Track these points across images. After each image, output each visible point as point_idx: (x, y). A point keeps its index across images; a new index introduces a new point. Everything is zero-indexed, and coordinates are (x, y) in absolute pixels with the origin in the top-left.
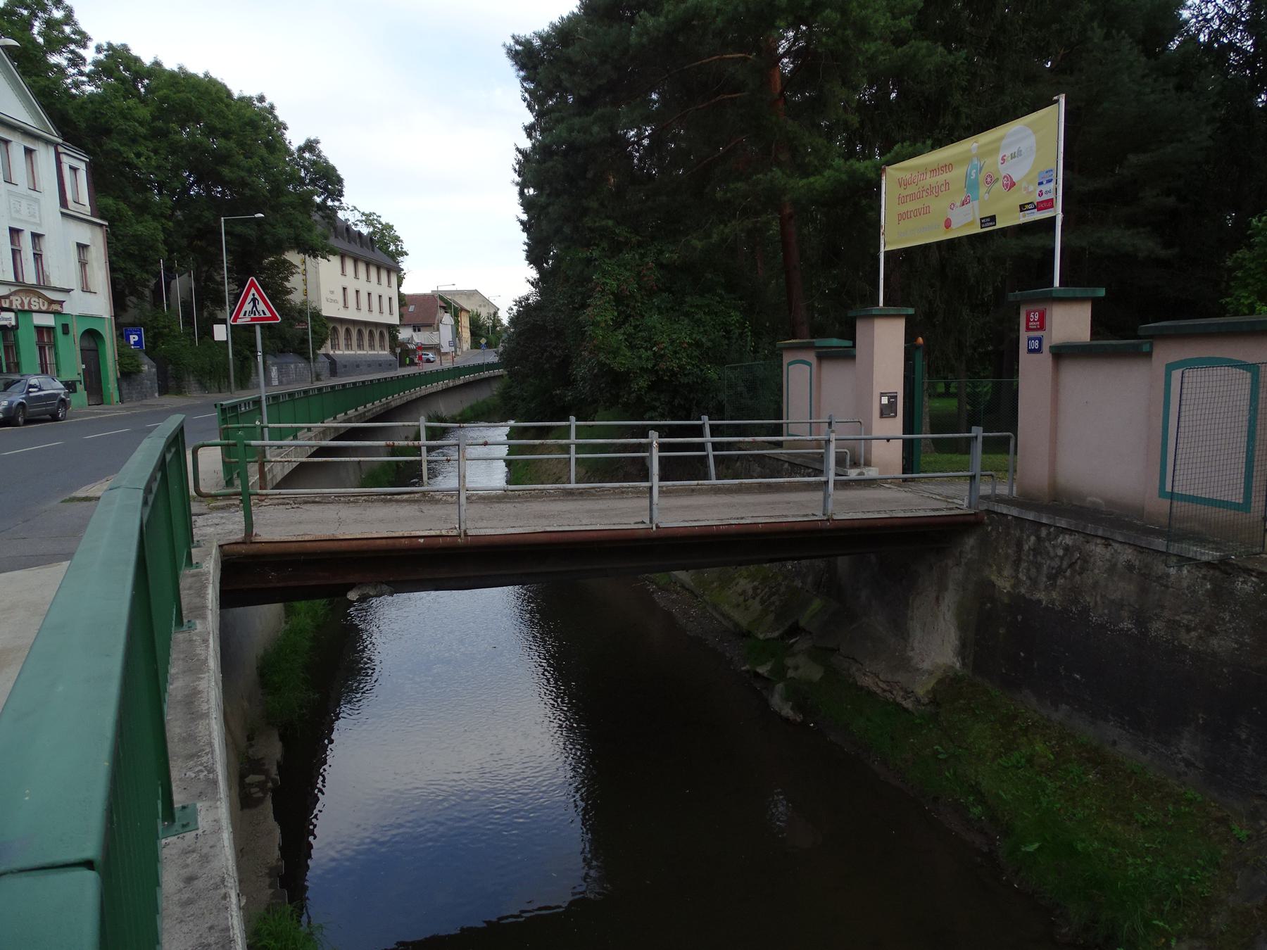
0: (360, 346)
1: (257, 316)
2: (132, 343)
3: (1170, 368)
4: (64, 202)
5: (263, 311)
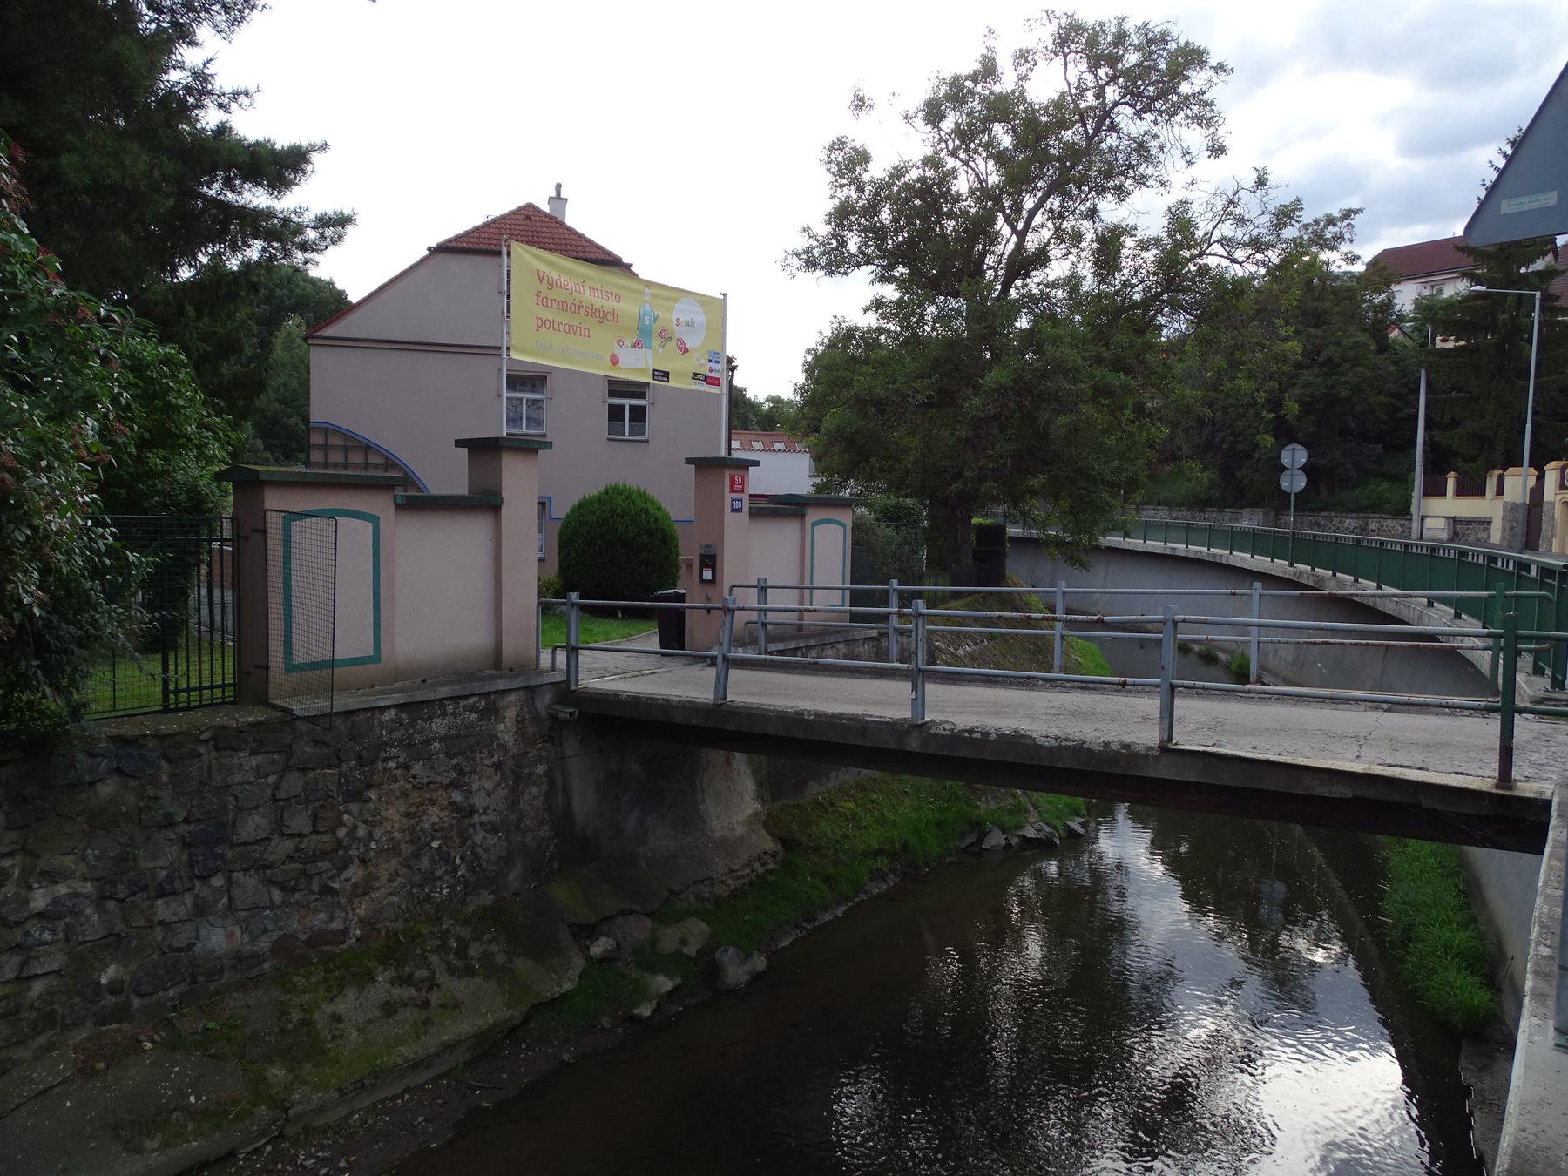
3: (814, 524)
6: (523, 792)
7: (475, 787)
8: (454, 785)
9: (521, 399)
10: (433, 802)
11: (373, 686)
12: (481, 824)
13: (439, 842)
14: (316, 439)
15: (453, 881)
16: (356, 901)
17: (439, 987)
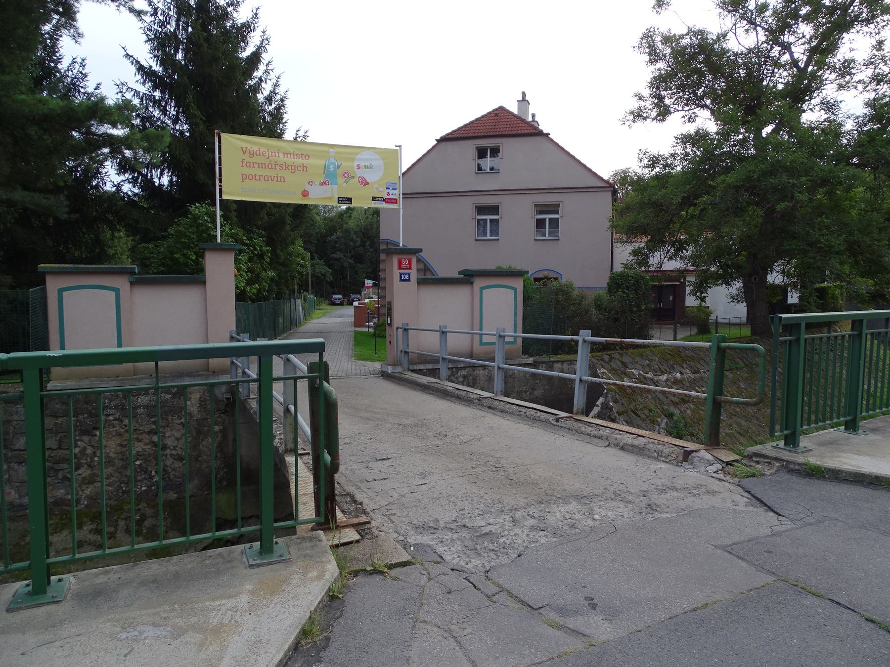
3: (482, 289)
6: (203, 440)
7: (167, 434)
8: (151, 432)
9: (486, 220)
10: (140, 441)
11: (118, 377)
12: (171, 455)
13: (140, 462)
14: (383, 247)
15: (149, 483)
16: (84, 487)
17: (115, 538)
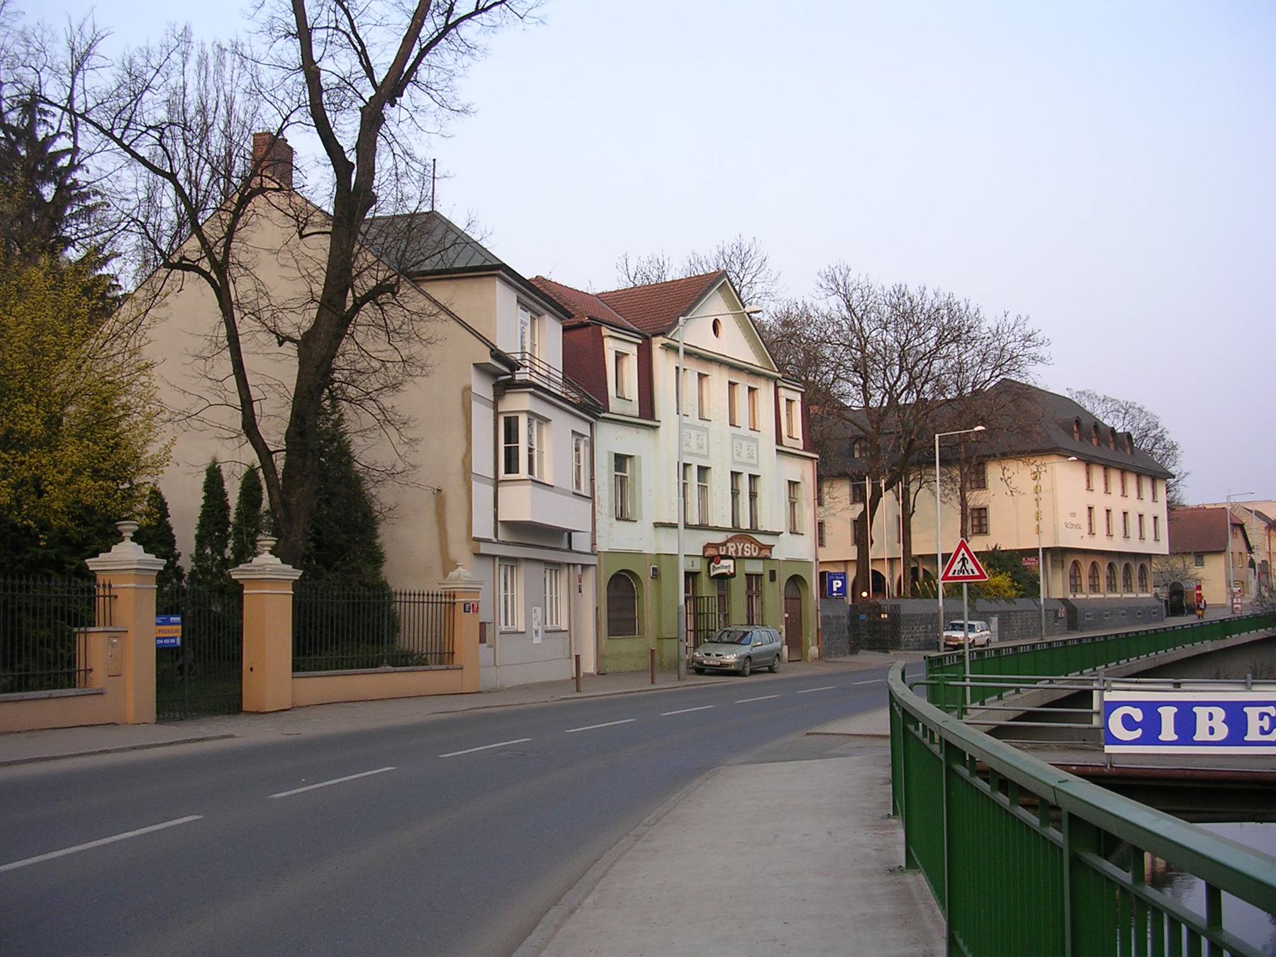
0: (1111, 587)
1: (966, 574)
2: (835, 590)
4: (779, 441)
5: (972, 570)
